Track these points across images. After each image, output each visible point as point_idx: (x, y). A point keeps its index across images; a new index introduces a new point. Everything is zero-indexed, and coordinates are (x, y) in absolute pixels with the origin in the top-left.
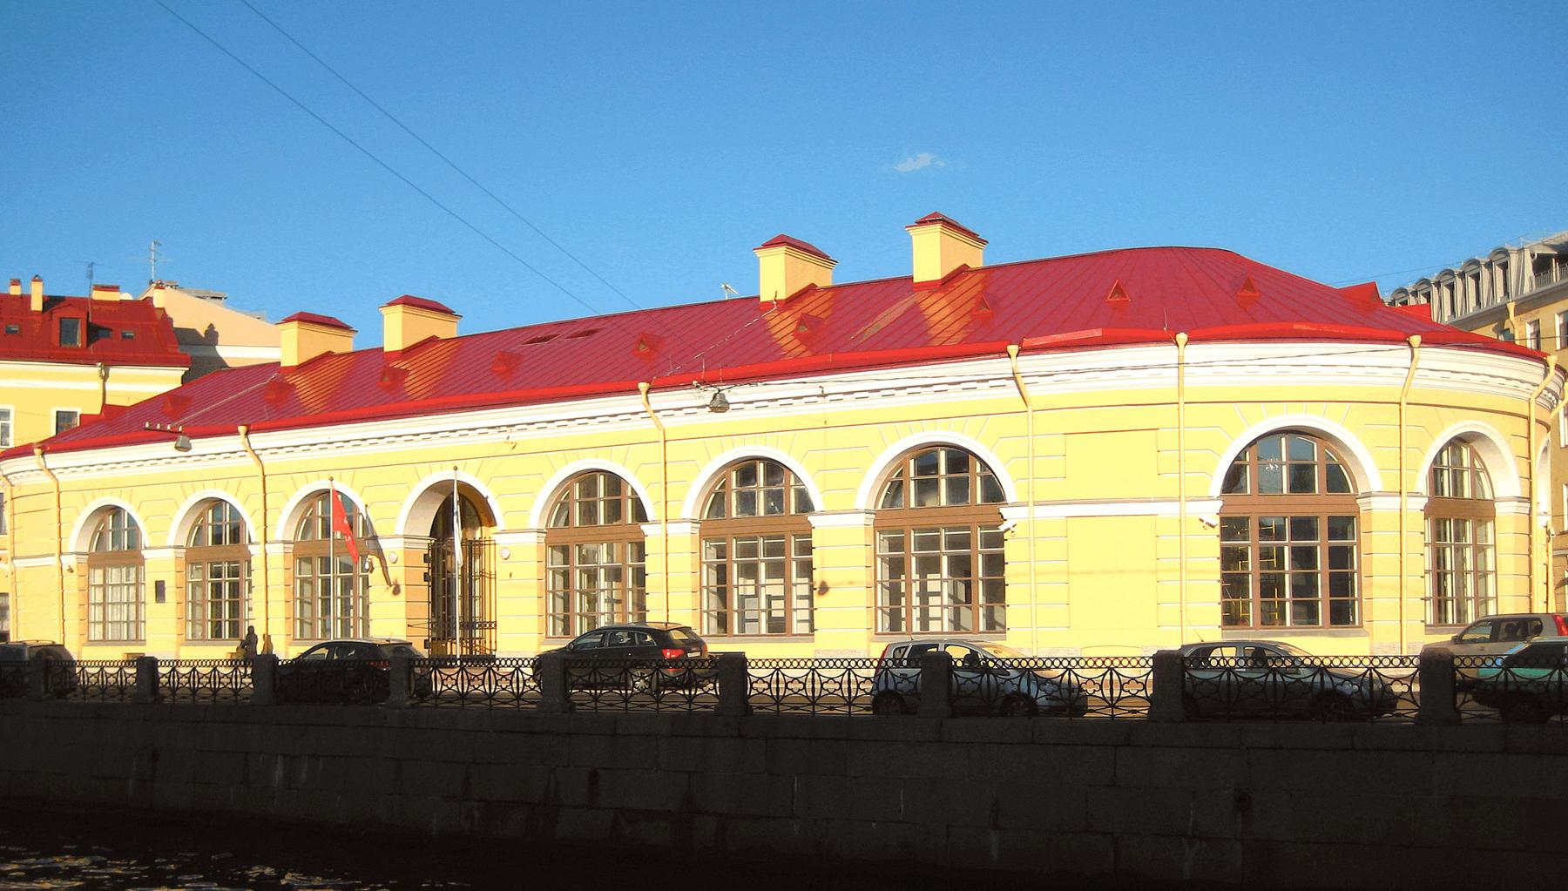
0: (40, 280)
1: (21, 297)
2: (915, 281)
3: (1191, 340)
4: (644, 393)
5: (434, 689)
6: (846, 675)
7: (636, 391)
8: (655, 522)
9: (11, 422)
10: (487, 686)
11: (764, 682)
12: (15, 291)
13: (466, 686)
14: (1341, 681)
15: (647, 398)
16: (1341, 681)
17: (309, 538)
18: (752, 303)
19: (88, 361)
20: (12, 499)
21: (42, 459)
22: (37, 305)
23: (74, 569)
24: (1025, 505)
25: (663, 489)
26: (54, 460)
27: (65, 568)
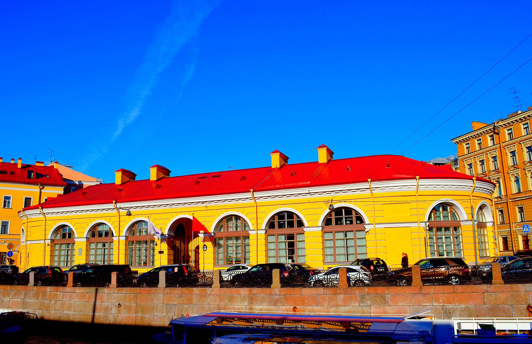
0: (21, 159)
1: (15, 164)
2: (319, 163)
3: (420, 178)
4: (252, 192)
5: (133, 282)
6: (358, 274)
7: (367, 181)
8: (116, 237)
9: (11, 200)
10: (203, 280)
11: (210, 278)
12: (13, 162)
13: (205, 280)
14: (352, 276)
15: (253, 194)
16: (352, 276)
17: (430, 220)
18: (269, 169)
19: (35, 184)
20: (28, 222)
21: (115, 205)
22: (19, 166)
23: (50, 244)
24: (417, 222)
25: (256, 220)
26: (46, 211)
27: (47, 244)
